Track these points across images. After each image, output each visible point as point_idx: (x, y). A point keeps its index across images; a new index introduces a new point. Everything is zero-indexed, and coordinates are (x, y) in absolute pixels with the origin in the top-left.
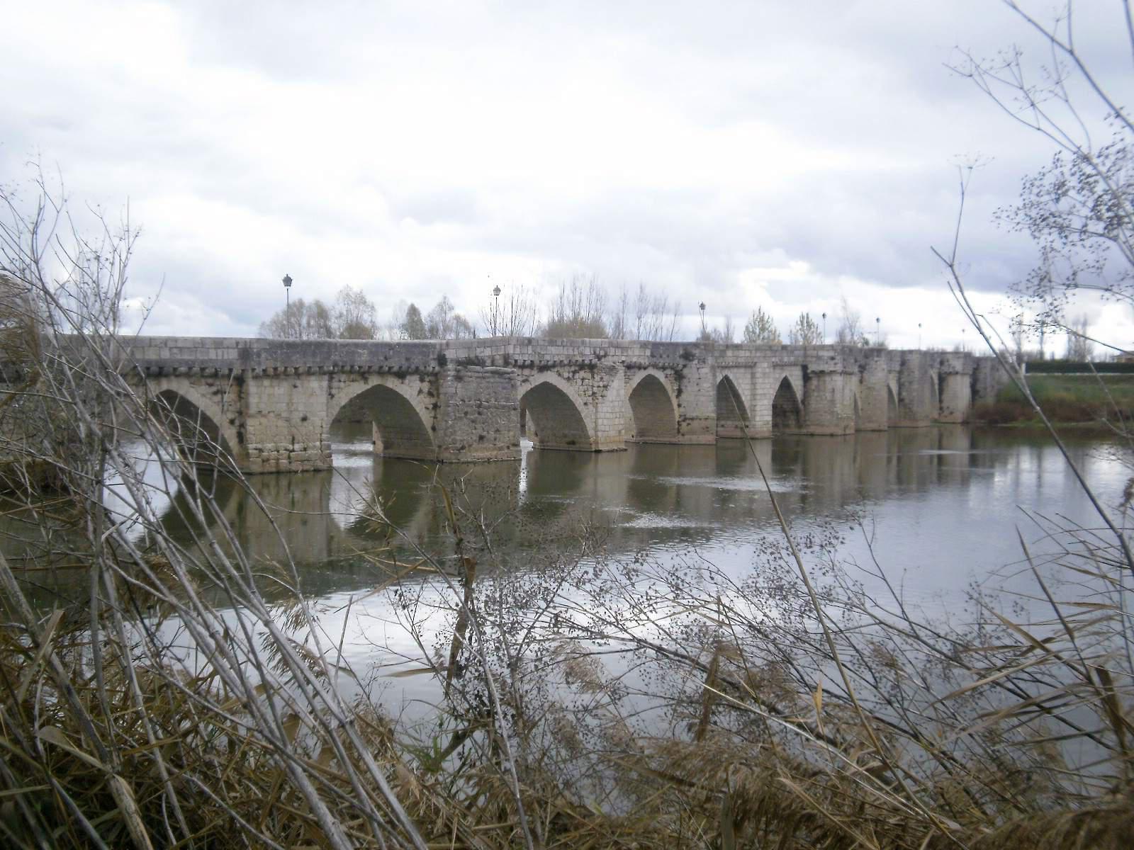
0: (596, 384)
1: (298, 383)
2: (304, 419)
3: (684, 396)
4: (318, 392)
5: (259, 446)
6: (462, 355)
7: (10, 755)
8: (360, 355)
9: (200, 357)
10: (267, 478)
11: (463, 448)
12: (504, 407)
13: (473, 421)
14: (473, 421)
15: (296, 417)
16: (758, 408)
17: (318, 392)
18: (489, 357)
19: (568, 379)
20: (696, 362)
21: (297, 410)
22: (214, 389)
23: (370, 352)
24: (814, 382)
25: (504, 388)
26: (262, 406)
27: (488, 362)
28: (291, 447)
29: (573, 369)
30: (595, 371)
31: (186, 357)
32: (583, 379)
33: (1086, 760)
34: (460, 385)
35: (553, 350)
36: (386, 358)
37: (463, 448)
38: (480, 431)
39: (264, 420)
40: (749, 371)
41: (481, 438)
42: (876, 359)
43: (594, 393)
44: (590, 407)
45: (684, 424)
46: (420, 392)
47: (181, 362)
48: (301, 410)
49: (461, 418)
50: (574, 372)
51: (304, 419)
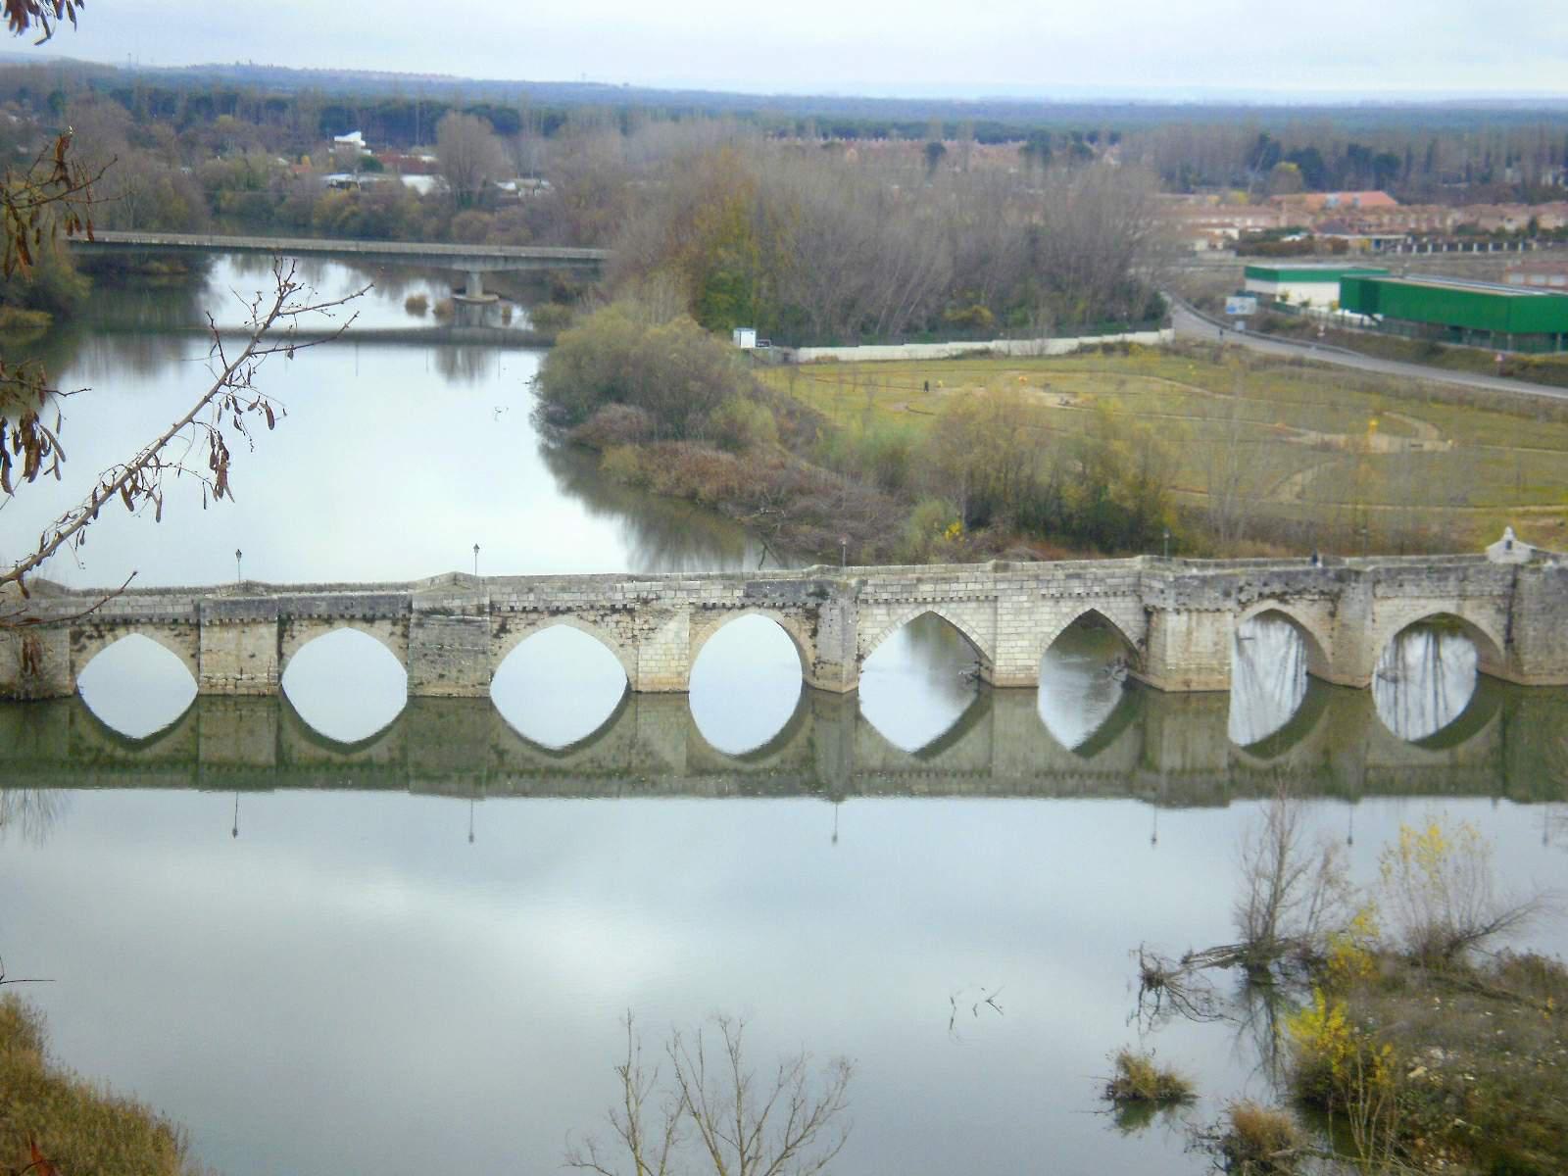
0: (637, 627)
1: (246, 629)
2: (253, 656)
3: (820, 636)
4: (267, 635)
5: (210, 675)
6: (426, 605)
7: (1378, 1064)
8: (319, 606)
9: (158, 611)
10: (213, 699)
11: (421, 684)
12: (468, 651)
13: (432, 662)
14: (432, 662)
15: (245, 654)
16: (999, 650)
17: (267, 635)
18: (458, 607)
19: (595, 622)
20: (829, 601)
21: (246, 649)
22: (176, 632)
23: (329, 605)
24: (1154, 618)
25: (470, 635)
26: (212, 646)
27: (458, 611)
28: (239, 676)
29: (602, 613)
30: (636, 614)
31: (146, 611)
32: (617, 622)
33: (758, 1167)
34: (421, 631)
35: (566, 596)
36: (347, 608)
37: (421, 684)
38: (440, 671)
39: (215, 656)
40: (987, 609)
41: (442, 676)
42: (1353, 584)
43: (634, 636)
44: (630, 649)
45: (819, 667)
46: (392, 634)
47: (141, 616)
48: (250, 650)
49: (419, 659)
50: (603, 616)
51: (253, 656)
